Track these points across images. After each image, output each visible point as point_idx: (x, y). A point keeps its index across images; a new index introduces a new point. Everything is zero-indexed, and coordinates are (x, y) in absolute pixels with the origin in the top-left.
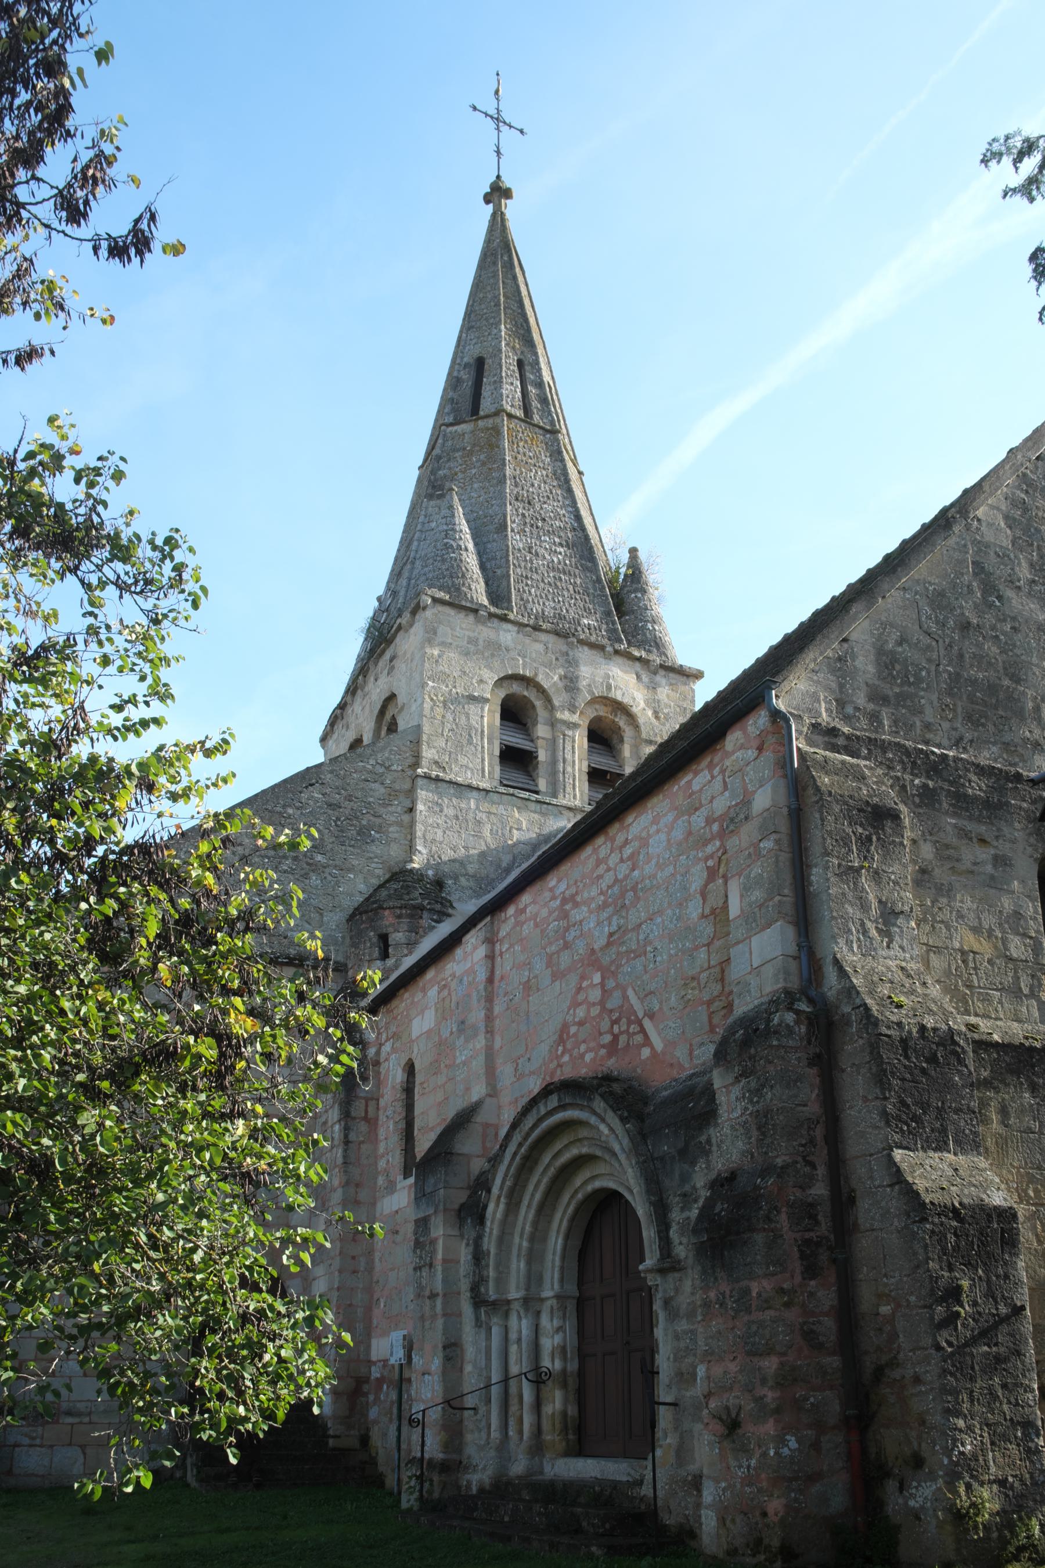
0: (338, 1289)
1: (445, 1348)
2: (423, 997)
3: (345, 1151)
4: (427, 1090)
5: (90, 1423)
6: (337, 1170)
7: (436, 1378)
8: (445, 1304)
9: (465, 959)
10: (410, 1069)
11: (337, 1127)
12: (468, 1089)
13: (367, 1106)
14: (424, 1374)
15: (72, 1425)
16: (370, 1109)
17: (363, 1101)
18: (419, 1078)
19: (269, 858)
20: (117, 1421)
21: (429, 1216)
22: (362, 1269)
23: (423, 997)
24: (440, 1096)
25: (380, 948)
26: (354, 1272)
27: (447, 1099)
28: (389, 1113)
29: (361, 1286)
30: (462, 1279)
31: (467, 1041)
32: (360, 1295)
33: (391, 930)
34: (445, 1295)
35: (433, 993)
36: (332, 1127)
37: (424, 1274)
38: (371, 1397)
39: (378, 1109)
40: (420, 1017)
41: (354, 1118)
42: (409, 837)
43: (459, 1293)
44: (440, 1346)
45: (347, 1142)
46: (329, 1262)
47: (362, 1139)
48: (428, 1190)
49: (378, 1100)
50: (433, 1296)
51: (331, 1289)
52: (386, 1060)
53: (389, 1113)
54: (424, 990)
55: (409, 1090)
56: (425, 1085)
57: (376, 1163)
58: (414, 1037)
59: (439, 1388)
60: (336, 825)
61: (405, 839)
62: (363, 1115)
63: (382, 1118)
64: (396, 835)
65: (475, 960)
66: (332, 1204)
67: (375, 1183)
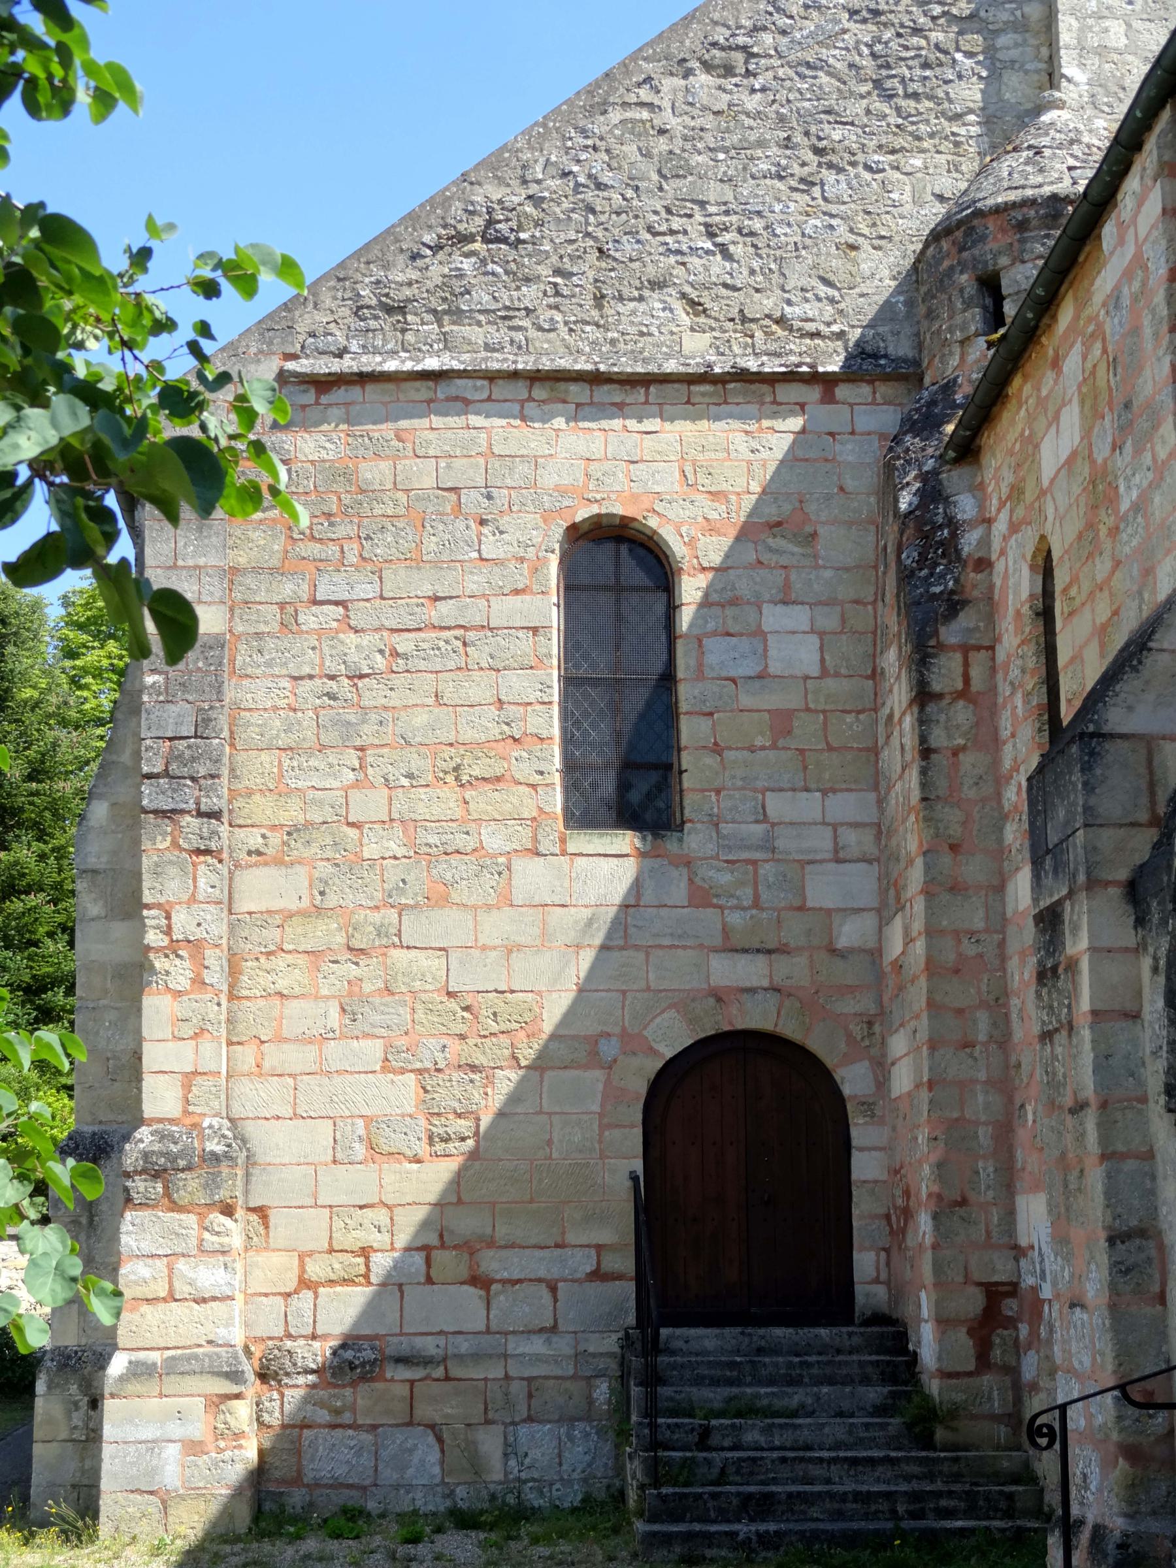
0: (931, 1085)
1: (1111, 1241)
2: (1056, 382)
3: (924, 772)
4: (1078, 602)
5: (447, 1378)
6: (912, 818)
7: (1097, 1320)
8: (1106, 1127)
9: (1121, 242)
10: (1046, 568)
11: (908, 721)
12: (1148, 572)
13: (966, 664)
14: (1072, 1306)
15: (412, 1382)
16: (975, 673)
17: (958, 657)
18: (1061, 578)
19: (726, 150)
20: (501, 1375)
21: (1060, 902)
22: (982, 1037)
23: (1056, 382)
24: (1103, 611)
25: (985, 308)
26: (965, 1046)
27: (1116, 613)
28: (1015, 673)
29: (982, 1076)
30: (1148, 1060)
31: (1138, 451)
32: (981, 1098)
33: (1004, 261)
34: (1104, 1105)
35: (1072, 364)
36: (900, 722)
37: (1059, 1050)
38: (1024, 1330)
39: (993, 670)
40: (1053, 429)
41: (940, 696)
42: (1045, 52)
43: (1144, 1100)
44: (1102, 1235)
45: (926, 752)
46: (913, 1023)
47: (961, 741)
48: (1053, 838)
49: (992, 648)
50: (1079, 1108)
51: (918, 1086)
52: (1003, 553)
53: (1015, 673)
54: (1056, 364)
55: (1046, 614)
56: (1073, 592)
57: (999, 796)
58: (1045, 483)
59: (1105, 1345)
60: (873, 55)
61: (1037, 57)
62: (959, 685)
63: (1004, 689)
64: (1014, 53)
65: (1142, 234)
66: (909, 895)
67: (1000, 840)
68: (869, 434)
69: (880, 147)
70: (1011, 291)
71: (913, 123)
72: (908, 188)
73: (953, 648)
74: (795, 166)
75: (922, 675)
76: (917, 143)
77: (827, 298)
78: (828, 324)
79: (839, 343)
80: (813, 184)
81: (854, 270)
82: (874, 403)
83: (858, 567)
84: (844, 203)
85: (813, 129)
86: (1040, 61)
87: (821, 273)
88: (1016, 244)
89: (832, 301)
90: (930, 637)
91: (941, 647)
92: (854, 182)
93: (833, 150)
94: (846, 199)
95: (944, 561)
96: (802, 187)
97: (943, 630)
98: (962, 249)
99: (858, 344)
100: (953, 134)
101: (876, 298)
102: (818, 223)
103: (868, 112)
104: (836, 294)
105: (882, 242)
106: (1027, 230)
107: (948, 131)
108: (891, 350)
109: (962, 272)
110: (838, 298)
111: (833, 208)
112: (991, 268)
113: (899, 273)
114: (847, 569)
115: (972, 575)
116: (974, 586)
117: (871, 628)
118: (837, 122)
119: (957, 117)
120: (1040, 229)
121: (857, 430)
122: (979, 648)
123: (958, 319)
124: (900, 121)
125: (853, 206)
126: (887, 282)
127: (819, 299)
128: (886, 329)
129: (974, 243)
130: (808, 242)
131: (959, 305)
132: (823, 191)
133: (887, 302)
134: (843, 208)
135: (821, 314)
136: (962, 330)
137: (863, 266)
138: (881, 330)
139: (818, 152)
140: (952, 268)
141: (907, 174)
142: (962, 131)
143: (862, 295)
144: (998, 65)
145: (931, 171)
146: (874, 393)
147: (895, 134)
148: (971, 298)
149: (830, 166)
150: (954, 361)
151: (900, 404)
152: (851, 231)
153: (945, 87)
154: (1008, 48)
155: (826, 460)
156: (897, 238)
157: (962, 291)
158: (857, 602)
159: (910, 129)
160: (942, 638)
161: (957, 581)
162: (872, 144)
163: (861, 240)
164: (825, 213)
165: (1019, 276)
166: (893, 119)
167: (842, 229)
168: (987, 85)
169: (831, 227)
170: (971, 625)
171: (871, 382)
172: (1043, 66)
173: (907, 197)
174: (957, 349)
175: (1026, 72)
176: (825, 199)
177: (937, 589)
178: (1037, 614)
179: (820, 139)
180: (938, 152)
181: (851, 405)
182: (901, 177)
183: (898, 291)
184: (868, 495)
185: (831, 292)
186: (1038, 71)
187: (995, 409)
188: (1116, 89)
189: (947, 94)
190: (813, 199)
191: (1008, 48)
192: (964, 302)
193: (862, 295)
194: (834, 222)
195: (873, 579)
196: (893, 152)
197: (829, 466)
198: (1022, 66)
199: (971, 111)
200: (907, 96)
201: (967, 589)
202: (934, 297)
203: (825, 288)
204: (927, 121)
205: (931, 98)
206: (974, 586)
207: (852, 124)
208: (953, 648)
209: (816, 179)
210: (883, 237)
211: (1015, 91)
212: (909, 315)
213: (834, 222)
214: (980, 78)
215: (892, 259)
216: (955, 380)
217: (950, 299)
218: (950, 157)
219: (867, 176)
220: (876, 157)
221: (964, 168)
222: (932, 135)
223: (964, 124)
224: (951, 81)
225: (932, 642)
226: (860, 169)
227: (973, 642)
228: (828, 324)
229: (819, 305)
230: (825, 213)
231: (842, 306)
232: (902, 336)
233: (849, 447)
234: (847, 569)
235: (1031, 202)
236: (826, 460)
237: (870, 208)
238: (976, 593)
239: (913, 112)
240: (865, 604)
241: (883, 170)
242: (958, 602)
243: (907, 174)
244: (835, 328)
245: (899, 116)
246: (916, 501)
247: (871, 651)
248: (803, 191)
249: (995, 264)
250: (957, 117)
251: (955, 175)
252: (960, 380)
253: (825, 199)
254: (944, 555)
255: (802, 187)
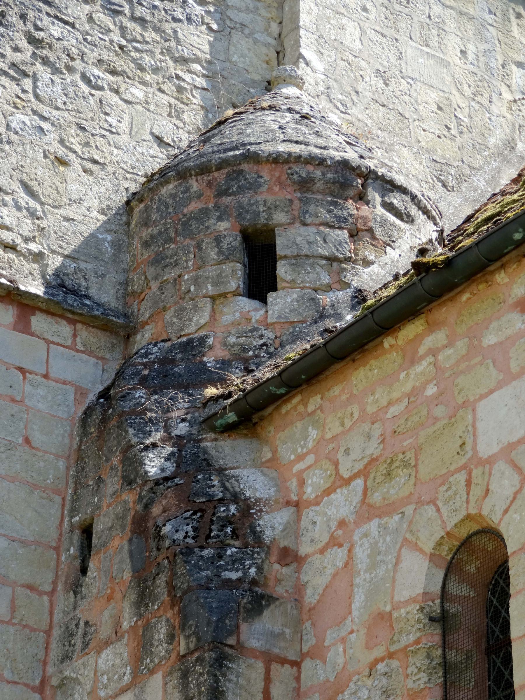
13: (268, 679)
17: (260, 665)
33: (280, 217)
68: (64, 383)
69: (100, 62)
70: (288, 252)
71: (137, 50)
72: (126, 117)
73: (254, 653)
74: (8, 48)
75: (217, 681)
76: (139, 73)
77: (28, 209)
78: (27, 240)
79: (35, 266)
80: (26, 75)
81: (61, 187)
82: (73, 347)
83: (37, 543)
84: (58, 109)
85: (31, 14)
86: (269, 35)
87: (25, 177)
88: (296, 202)
89: (33, 214)
90: (230, 633)
91: (239, 647)
92: (70, 89)
93: (50, 47)
94: (61, 106)
95: (237, 543)
96: (12, 73)
97: (244, 627)
98: (222, 193)
99: (57, 273)
100: (178, 77)
101: (83, 228)
102: (26, 119)
103: (91, 19)
104: (39, 208)
105: (95, 168)
106: (309, 190)
107: (172, 72)
108: (92, 292)
109: (220, 219)
110: (39, 213)
111: (45, 111)
112: (263, 221)
113: (109, 208)
114: (24, 543)
115: (276, 566)
116: (278, 581)
117: (45, 626)
118: (56, 17)
119: (183, 61)
120: (323, 193)
121: (52, 375)
122: (283, 661)
123: (211, 271)
124: (124, 42)
125: (66, 114)
126: (94, 214)
127: (19, 208)
128: (90, 266)
129: (241, 190)
130: (14, 137)
131: (213, 254)
132: (35, 87)
133: (93, 236)
134: (55, 113)
135: (19, 225)
136: (216, 284)
137: (71, 186)
138: (83, 265)
139: (33, 41)
140: (205, 212)
141: (126, 101)
142: (187, 77)
143: (67, 219)
144: (228, 22)
145: (152, 108)
146: (75, 336)
147: (117, 55)
148: (232, 249)
149: (45, 62)
150: (204, 317)
151: (102, 358)
152: (62, 142)
153: (174, 25)
154: (239, 10)
155: (13, 400)
156: (110, 168)
157: (218, 240)
158: (31, 588)
159: (133, 54)
160: (243, 637)
161: (260, 569)
162: (93, 56)
163: (71, 156)
164: (35, 112)
165: (299, 239)
166: (116, 37)
167: (52, 137)
168: (215, 38)
169: (41, 129)
170: (277, 629)
171: (72, 322)
172: (273, 42)
173: (124, 126)
174: (207, 306)
175: (256, 41)
176: (37, 96)
177: (234, 576)
178: (432, 619)
179: (38, 29)
180: (160, 90)
181: (48, 342)
182: (121, 102)
183: (106, 227)
184: (57, 456)
185: (33, 204)
186: (267, 45)
187: (337, 366)
188: (349, 89)
189: (175, 32)
190: (24, 91)
191: (239, 10)
192: (220, 252)
193: (67, 219)
194: (45, 125)
195: (53, 563)
196: (113, 72)
197: (15, 408)
198: (251, 34)
199: (198, 60)
200: (133, 18)
201: (271, 583)
202: (170, 240)
203: (27, 198)
204: (152, 53)
205: (158, 30)
206: (278, 581)
207: (73, 26)
208: (254, 653)
209: (29, 70)
210: (95, 162)
211: (242, 56)
212: (115, 260)
213: (45, 125)
214: (210, 29)
215: (103, 190)
216: (202, 340)
217: (199, 246)
218: (173, 101)
219: (85, 88)
220: (96, 72)
221: (185, 116)
222: (156, 70)
223: (190, 71)
224: (180, 21)
225: (231, 641)
226: (77, 77)
227: (276, 651)
228: (27, 240)
229: (18, 214)
230: (35, 112)
231: (44, 224)
232: (106, 280)
233: (41, 391)
234: (24, 543)
235: (321, 162)
236: (13, 400)
237: (85, 124)
238: (280, 591)
239: (139, 38)
240: (41, 593)
241: (101, 89)
242: (262, 597)
243: (126, 101)
244: (34, 247)
245: (123, 37)
246: (171, 467)
247: (41, 655)
248: (13, 79)
249: (268, 219)
250: (183, 61)
251: (177, 122)
252: (210, 341)
253: (37, 96)
254: (235, 535)
255: (12, 73)
